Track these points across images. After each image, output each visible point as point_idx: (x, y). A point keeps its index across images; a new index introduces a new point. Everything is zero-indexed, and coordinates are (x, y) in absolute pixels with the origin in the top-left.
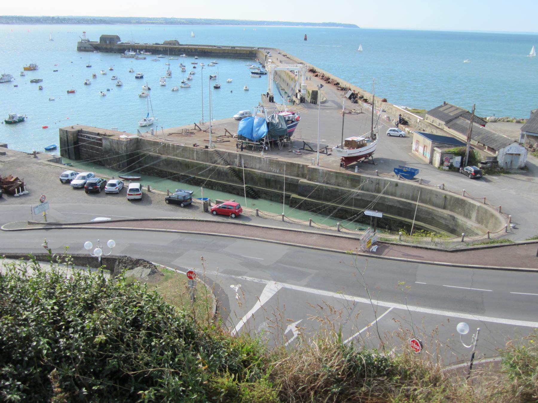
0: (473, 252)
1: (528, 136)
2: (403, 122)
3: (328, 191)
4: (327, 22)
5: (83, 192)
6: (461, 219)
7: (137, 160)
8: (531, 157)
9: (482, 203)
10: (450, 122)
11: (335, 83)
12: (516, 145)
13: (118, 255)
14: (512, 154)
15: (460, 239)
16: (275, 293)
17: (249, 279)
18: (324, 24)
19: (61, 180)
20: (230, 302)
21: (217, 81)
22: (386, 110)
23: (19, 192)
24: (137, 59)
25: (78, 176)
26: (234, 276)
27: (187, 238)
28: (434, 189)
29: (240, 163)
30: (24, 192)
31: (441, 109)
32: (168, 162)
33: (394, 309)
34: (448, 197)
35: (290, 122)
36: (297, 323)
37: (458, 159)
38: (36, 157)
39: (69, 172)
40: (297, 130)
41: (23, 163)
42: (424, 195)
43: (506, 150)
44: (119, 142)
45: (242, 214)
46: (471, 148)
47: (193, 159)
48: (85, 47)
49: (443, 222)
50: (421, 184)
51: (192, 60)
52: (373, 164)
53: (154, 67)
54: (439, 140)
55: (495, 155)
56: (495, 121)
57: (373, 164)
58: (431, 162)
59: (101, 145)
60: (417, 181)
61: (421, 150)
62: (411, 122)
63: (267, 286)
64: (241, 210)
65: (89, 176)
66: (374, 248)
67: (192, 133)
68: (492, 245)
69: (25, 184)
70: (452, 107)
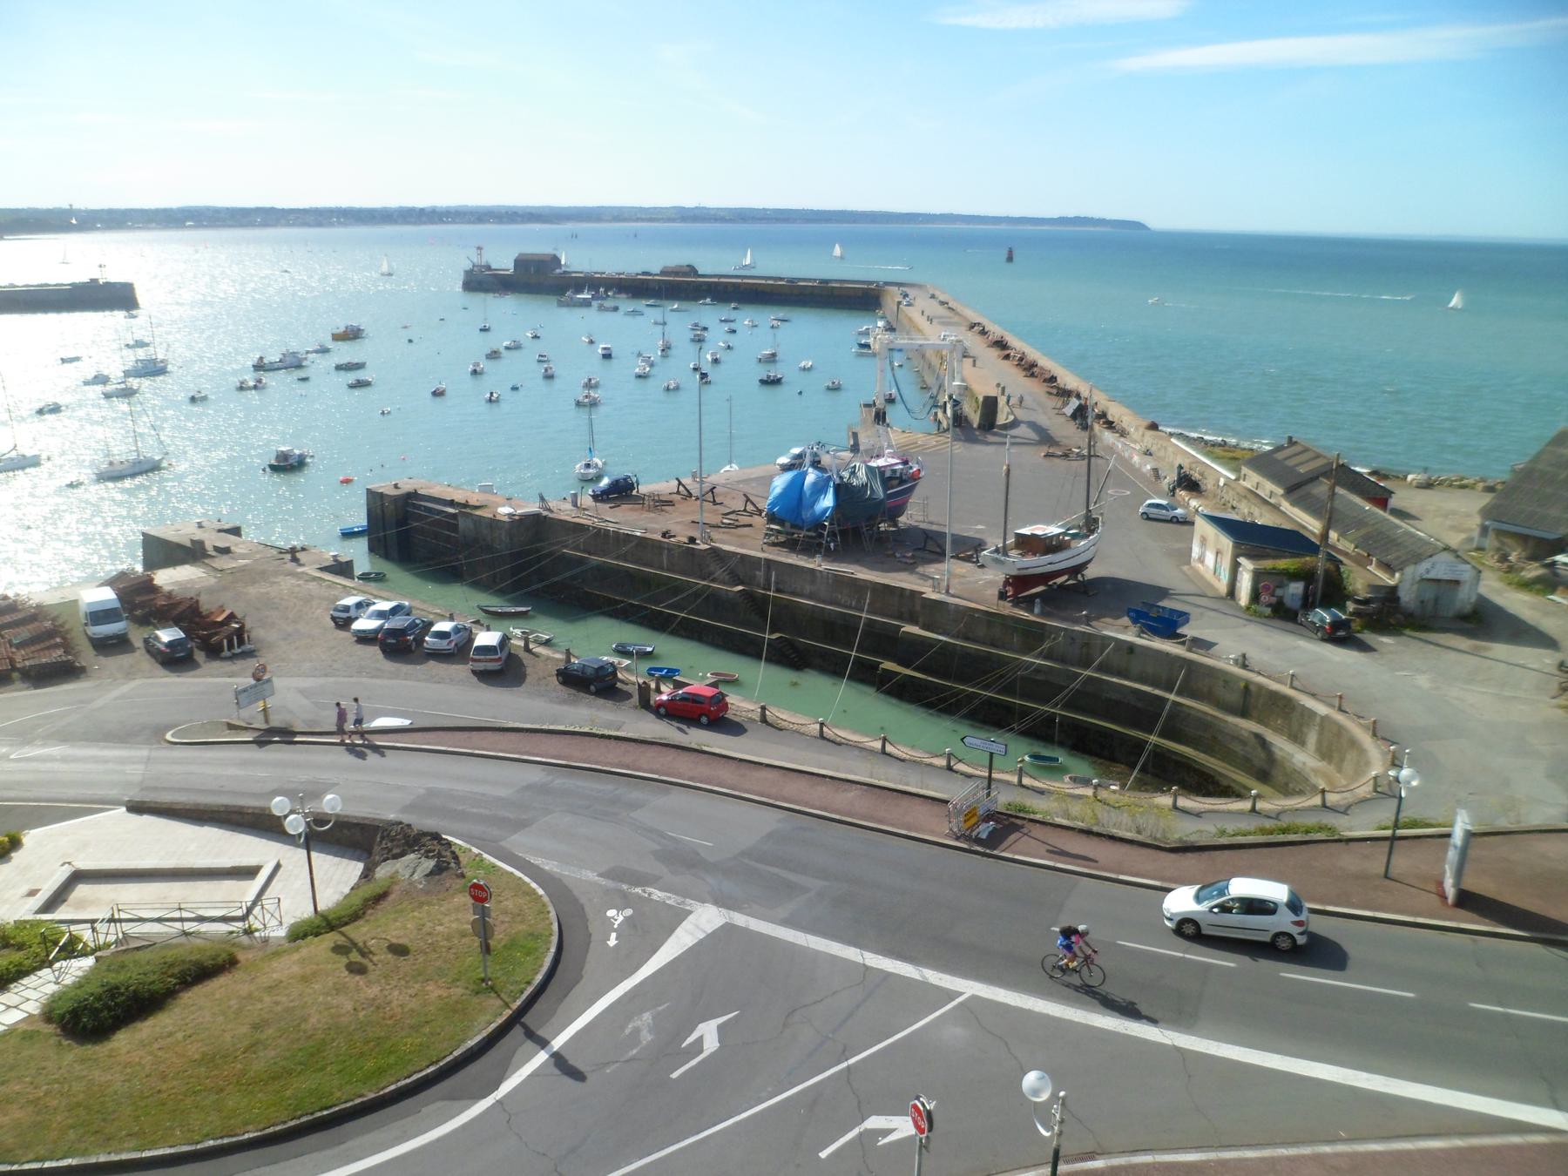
0: (1227, 853)
1: (1500, 533)
2: (1189, 483)
3: (967, 655)
4: (1071, 213)
5: (375, 651)
6: (1281, 744)
7: (537, 565)
8: (1497, 585)
9: (1332, 706)
10: (1296, 488)
11: (1047, 376)
12: (1446, 556)
13: (392, 816)
14: (1439, 581)
15: (1246, 805)
16: (702, 936)
17: (657, 895)
18: (1063, 221)
19: (333, 618)
20: (589, 956)
21: (778, 365)
22: (1153, 449)
23: (231, 646)
24: (601, 308)
25: (372, 608)
26: (625, 887)
27: (562, 781)
28: (1220, 665)
29: (768, 580)
30: (243, 648)
31: (1280, 456)
32: (604, 573)
33: (974, 998)
34: (1252, 688)
35: (895, 482)
36: (721, 1020)
37: (1296, 588)
38: (295, 560)
39: (350, 601)
40: (914, 499)
41: (263, 573)
42: (1197, 680)
43: (1422, 569)
44: (494, 523)
45: (729, 715)
46: (1331, 558)
47: (661, 568)
48: (480, 282)
49: (1237, 747)
50: (1190, 650)
51: (726, 311)
52: (1085, 593)
53: (636, 329)
54: (1248, 537)
55: (1391, 583)
56: (1428, 485)
57: (1085, 593)
58: (1232, 593)
59: (455, 528)
60: (1183, 643)
61: (1210, 557)
62: (1208, 485)
63: (691, 917)
64: (725, 707)
65: (395, 611)
66: (984, 830)
67: (670, 503)
68: (1281, 838)
69: (247, 627)
70: (1306, 450)
